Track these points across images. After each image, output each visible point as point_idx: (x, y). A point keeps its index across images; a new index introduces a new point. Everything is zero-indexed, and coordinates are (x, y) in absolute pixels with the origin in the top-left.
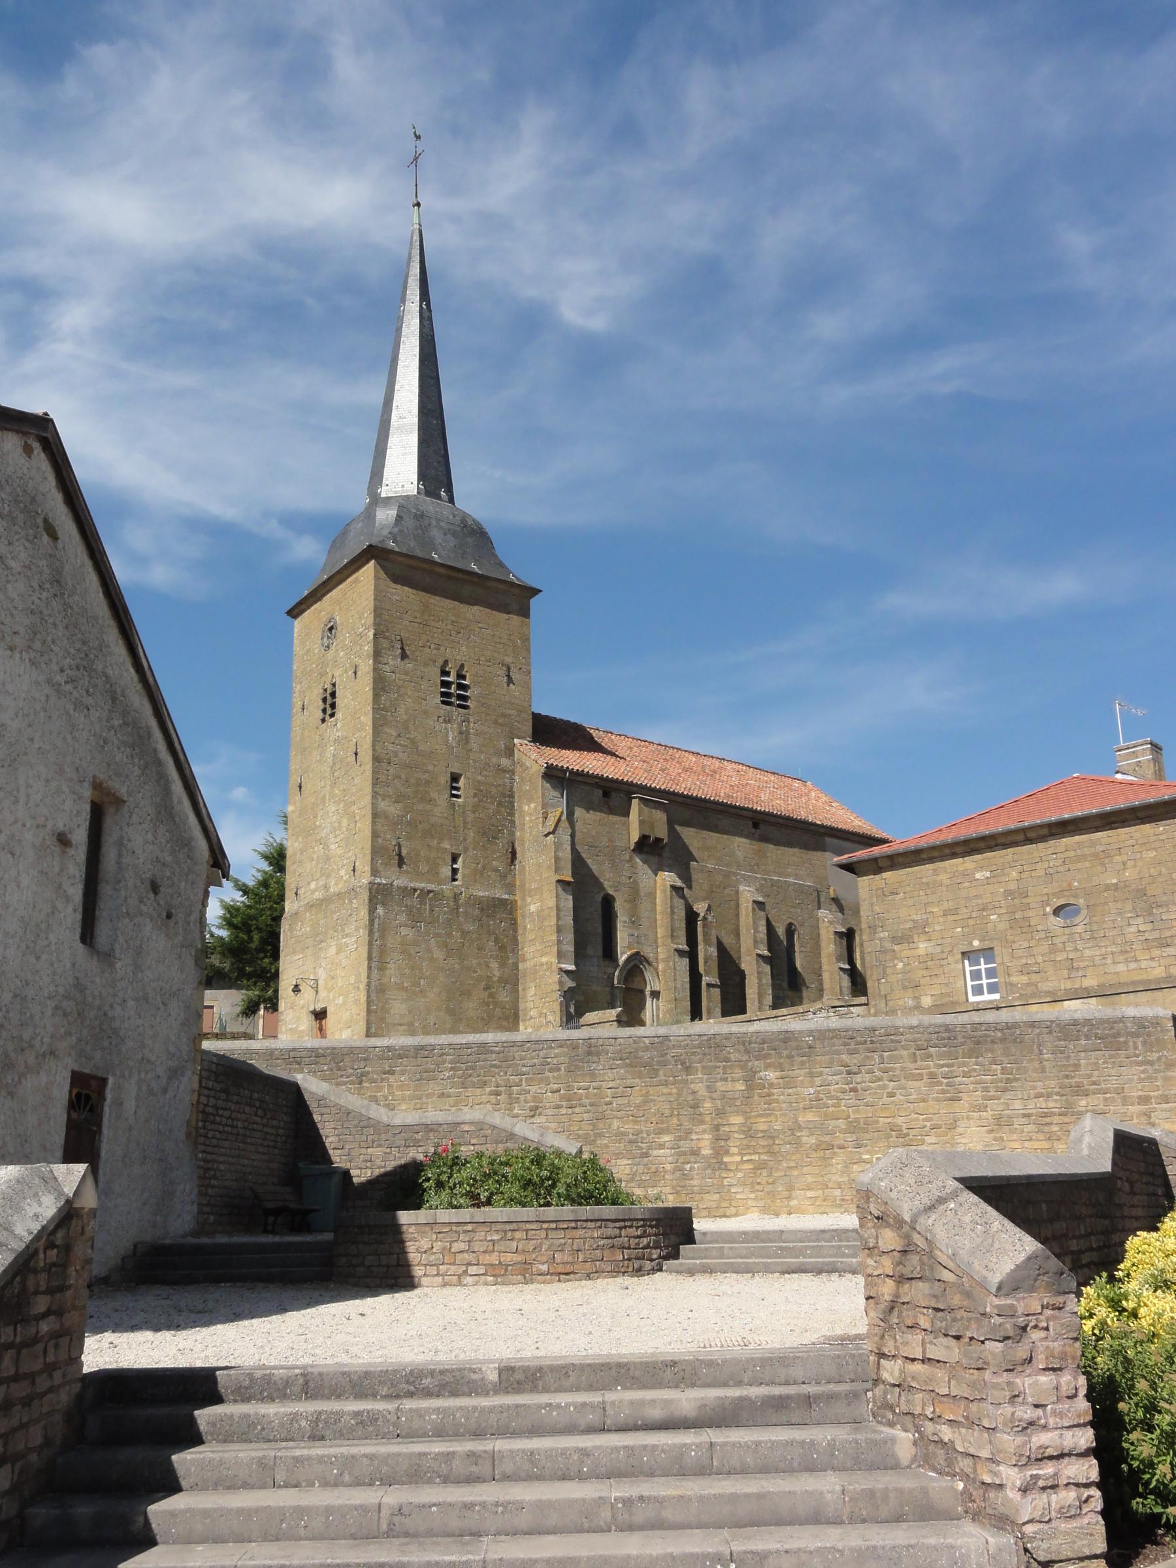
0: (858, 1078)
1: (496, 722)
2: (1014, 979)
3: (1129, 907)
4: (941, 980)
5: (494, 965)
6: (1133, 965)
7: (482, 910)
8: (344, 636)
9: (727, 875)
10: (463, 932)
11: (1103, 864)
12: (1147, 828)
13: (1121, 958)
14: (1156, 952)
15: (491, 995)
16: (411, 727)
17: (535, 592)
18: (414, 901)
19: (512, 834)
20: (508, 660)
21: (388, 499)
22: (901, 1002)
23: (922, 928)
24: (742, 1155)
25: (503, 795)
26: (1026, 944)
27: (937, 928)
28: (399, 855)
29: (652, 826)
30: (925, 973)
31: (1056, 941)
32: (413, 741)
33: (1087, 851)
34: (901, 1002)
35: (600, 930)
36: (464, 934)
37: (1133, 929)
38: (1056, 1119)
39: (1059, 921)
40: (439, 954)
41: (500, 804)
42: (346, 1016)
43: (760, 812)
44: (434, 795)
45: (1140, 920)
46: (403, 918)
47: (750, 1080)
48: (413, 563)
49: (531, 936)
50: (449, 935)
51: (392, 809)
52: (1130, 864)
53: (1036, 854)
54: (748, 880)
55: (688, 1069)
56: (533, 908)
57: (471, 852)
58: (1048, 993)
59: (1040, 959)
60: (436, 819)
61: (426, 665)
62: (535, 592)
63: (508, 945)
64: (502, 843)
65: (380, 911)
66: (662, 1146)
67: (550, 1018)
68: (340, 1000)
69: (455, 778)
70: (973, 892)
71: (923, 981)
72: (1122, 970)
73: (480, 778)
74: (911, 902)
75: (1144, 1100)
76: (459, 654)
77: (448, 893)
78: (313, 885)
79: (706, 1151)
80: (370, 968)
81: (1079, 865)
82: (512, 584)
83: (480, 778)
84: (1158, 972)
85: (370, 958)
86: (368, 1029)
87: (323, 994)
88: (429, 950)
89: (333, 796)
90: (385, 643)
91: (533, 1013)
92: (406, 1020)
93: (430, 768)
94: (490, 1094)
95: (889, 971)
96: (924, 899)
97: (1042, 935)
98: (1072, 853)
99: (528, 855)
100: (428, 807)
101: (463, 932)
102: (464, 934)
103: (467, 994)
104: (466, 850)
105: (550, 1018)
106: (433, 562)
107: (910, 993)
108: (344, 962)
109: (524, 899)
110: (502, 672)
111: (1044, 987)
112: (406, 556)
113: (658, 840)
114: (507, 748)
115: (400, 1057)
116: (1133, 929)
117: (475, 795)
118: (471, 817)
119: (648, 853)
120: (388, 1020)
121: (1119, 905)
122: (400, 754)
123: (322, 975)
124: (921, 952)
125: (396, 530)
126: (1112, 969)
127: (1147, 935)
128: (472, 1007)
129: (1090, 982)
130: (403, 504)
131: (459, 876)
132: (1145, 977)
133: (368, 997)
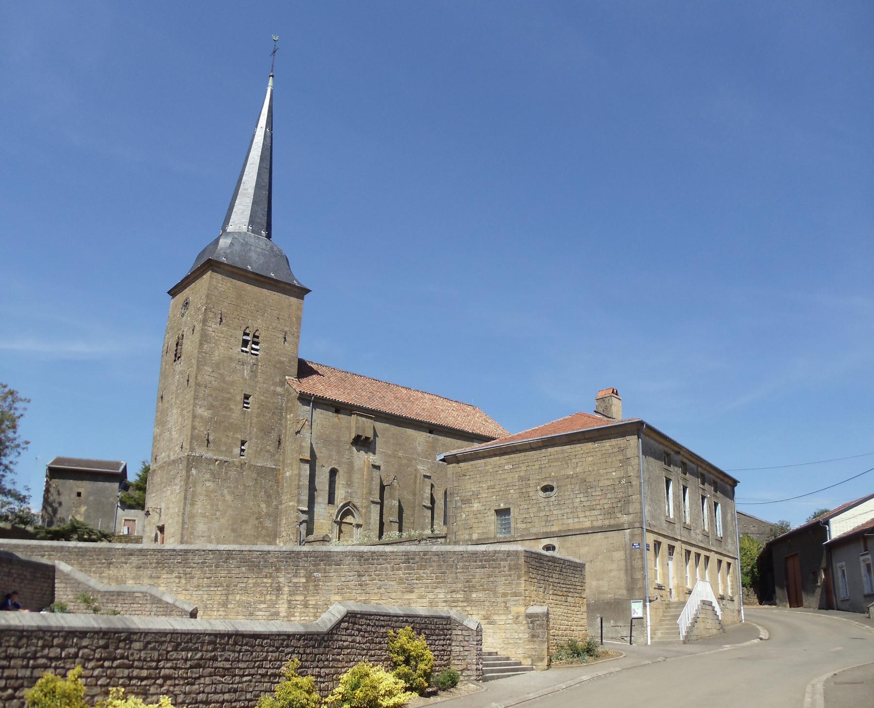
0: (363, 579)
1: (275, 366)
2: (519, 526)
3: (577, 488)
4: (483, 525)
5: (263, 506)
6: (576, 520)
7: (258, 474)
8: (191, 309)
9: (410, 460)
10: (245, 485)
11: (567, 463)
12: (590, 445)
13: (571, 516)
14: (588, 513)
15: (260, 523)
16: (221, 367)
17: (308, 291)
18: (214, 467)
19: (280, 431)
20: (287, 329)
21: (230, 233)
22: (462, 537)
23: (476, 495)
24: (301, 617)
25: (277, 408)
26: (526, 507)
27: (484, 495)
28: (208, 440)
29: (364, 430)
30: (476, 520)
31: (541, 505)
32: (221, 374)
33: (560, 456)
34: (462, 537)
35: (327, 488)
36: (246, 487)
37: (578, 500)
38: (460, 604)
39: (541, 493)
40: (228, 498)
41: (274, 413)
42: (173, 530)
43: (434, 424)
44: (233, 407)
45: (582, 495)
46: (208, 476)
47: (309, 577)
48: (234, 270)
49: (285, 490)
50: (236, 487)
51: (206, 414)
52: (580, 464)
53: (535, 457)
54: (423, 463)
55: (278, 570)
56: (288, 474)
57: (254, 440)
58: (535, 534)
59: (532, 515)
60: (231, 421)
61: (235, 329)
62: (308, 291)
63: (272, 495)
64: (274, 436)
65: (194, 471)
66: (260, 610)
67: (292, 537)
68: (170, 521)
69: (247, 397)
70: (503, 476)
71: (475, 525)
72: (572, 523)
73: (262, 398)
74: (472, 481)
75: (505, 595)
76: (257, 324)
77: (237, 463)
78: (163, 455)
79: (283, 614)
80: (185, 504)
81: (555, 464)
82: (294, 286)
83: (262, 398)
84: (588, 524)
85: (185, 498)
86: (182, 538)
87: (163, 517)
88: (223, 496)
89: (176, 403)
90: (211, 315)
91: (284, 534)
92: (206, 534)
93: (232, 391)
94: (176, 577)
95: (458, 519)
96: (479, 479)
97: (534, 502)
98: (552, 457)
99: (287, 444)
100: (229, 413)
101: (245, 485)
102: (246, 487)
103: (245, 521)
104: (251, 439)
105: (292, 537)
106: (246, 271)
107: (467, 532)
108: (174, 500)
109: (283, 469)
110: (282, 336)
111: (534, 530)
112: (231, 266)
113: (367, 438)
114: (280, 381)
115: (131, 555)
116: (578, 500)
117: (259, 408)
118: (255, 420)
119: (362, 445)
120: (195, 534)
121: (573, 486)
122: (213, 383)
123: (163, 506)
124: (475, 509)
125: (228, 251)
126: (566, 521)
127: (584, 504)
128: (248, 529)
129: (555, 529)
130: (235, 235)
131: (245, 453)
132: (581, 527)
133: (183, 520)
